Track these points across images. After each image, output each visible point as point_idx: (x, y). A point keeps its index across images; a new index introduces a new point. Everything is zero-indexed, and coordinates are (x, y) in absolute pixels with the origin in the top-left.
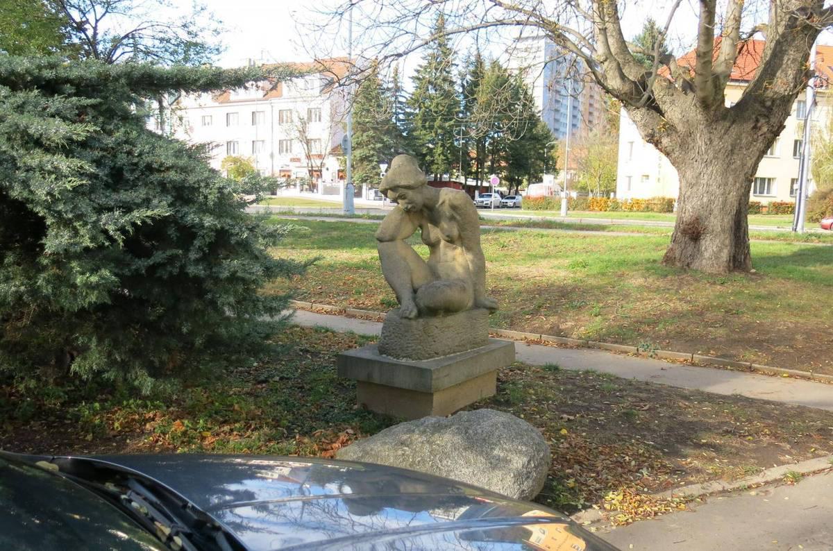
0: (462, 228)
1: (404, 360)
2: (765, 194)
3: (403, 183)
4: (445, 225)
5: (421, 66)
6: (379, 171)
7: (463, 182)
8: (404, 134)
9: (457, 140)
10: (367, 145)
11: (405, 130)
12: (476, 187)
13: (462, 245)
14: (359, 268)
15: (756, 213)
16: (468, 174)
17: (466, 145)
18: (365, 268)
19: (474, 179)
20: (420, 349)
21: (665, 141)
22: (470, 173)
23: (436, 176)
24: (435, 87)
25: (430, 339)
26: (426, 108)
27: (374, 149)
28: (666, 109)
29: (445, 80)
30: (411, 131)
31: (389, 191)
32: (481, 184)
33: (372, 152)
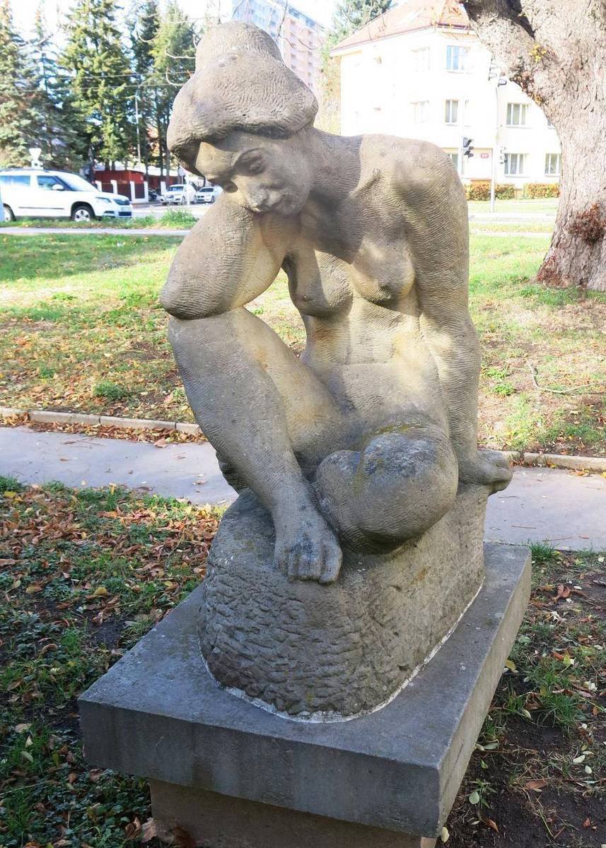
0: (427, 260)
1: (316, 719)
2: (518, 174)
3: (256, 115)
4: (374, 249)
5: (72, 10)
6: (29, 158)
7: (144, 171)
8: (60, 106)
9: (130, 114)
10: (8, 122)
11: (59, 100)
12: (161, 178)
13: (420, 308)
14: (36, 318)
15: (510, 198)
16: (148, 160)
17: (143, 120)
18: (47, 317)
19: (157, 166)
20: (363, 676)
21: (541, 80)
22: (152, 159)
23: (107, 164)
24: (95, 37)
25: (388, 632)
26: (86, 69)
27: (18, 128)
28: (539, 22)
29: (106, 29)
30: (67, 102)
31: (204, 146)
32: (168, 173)
33: (16, 132)
